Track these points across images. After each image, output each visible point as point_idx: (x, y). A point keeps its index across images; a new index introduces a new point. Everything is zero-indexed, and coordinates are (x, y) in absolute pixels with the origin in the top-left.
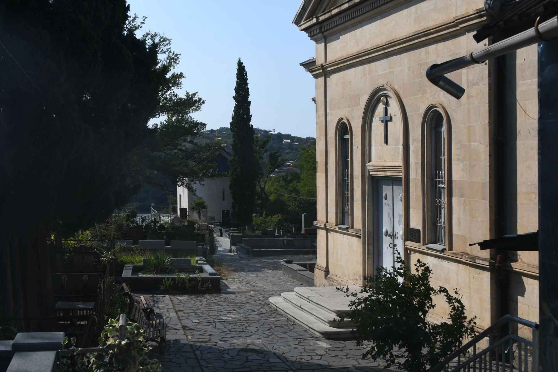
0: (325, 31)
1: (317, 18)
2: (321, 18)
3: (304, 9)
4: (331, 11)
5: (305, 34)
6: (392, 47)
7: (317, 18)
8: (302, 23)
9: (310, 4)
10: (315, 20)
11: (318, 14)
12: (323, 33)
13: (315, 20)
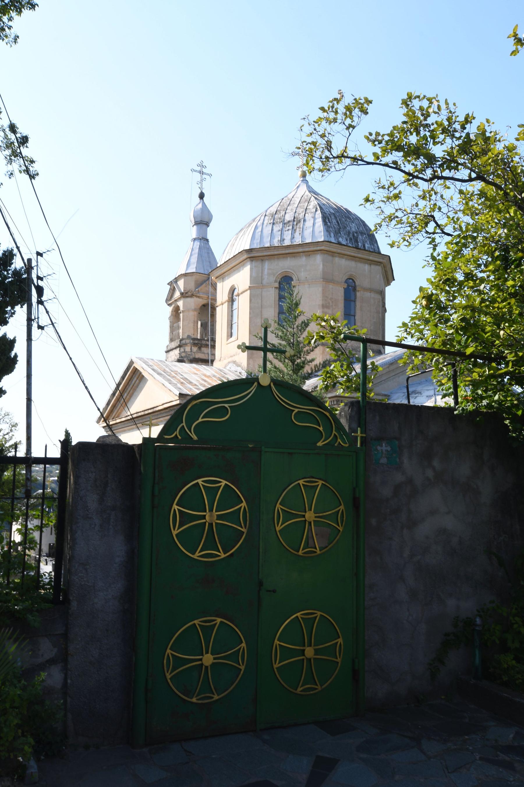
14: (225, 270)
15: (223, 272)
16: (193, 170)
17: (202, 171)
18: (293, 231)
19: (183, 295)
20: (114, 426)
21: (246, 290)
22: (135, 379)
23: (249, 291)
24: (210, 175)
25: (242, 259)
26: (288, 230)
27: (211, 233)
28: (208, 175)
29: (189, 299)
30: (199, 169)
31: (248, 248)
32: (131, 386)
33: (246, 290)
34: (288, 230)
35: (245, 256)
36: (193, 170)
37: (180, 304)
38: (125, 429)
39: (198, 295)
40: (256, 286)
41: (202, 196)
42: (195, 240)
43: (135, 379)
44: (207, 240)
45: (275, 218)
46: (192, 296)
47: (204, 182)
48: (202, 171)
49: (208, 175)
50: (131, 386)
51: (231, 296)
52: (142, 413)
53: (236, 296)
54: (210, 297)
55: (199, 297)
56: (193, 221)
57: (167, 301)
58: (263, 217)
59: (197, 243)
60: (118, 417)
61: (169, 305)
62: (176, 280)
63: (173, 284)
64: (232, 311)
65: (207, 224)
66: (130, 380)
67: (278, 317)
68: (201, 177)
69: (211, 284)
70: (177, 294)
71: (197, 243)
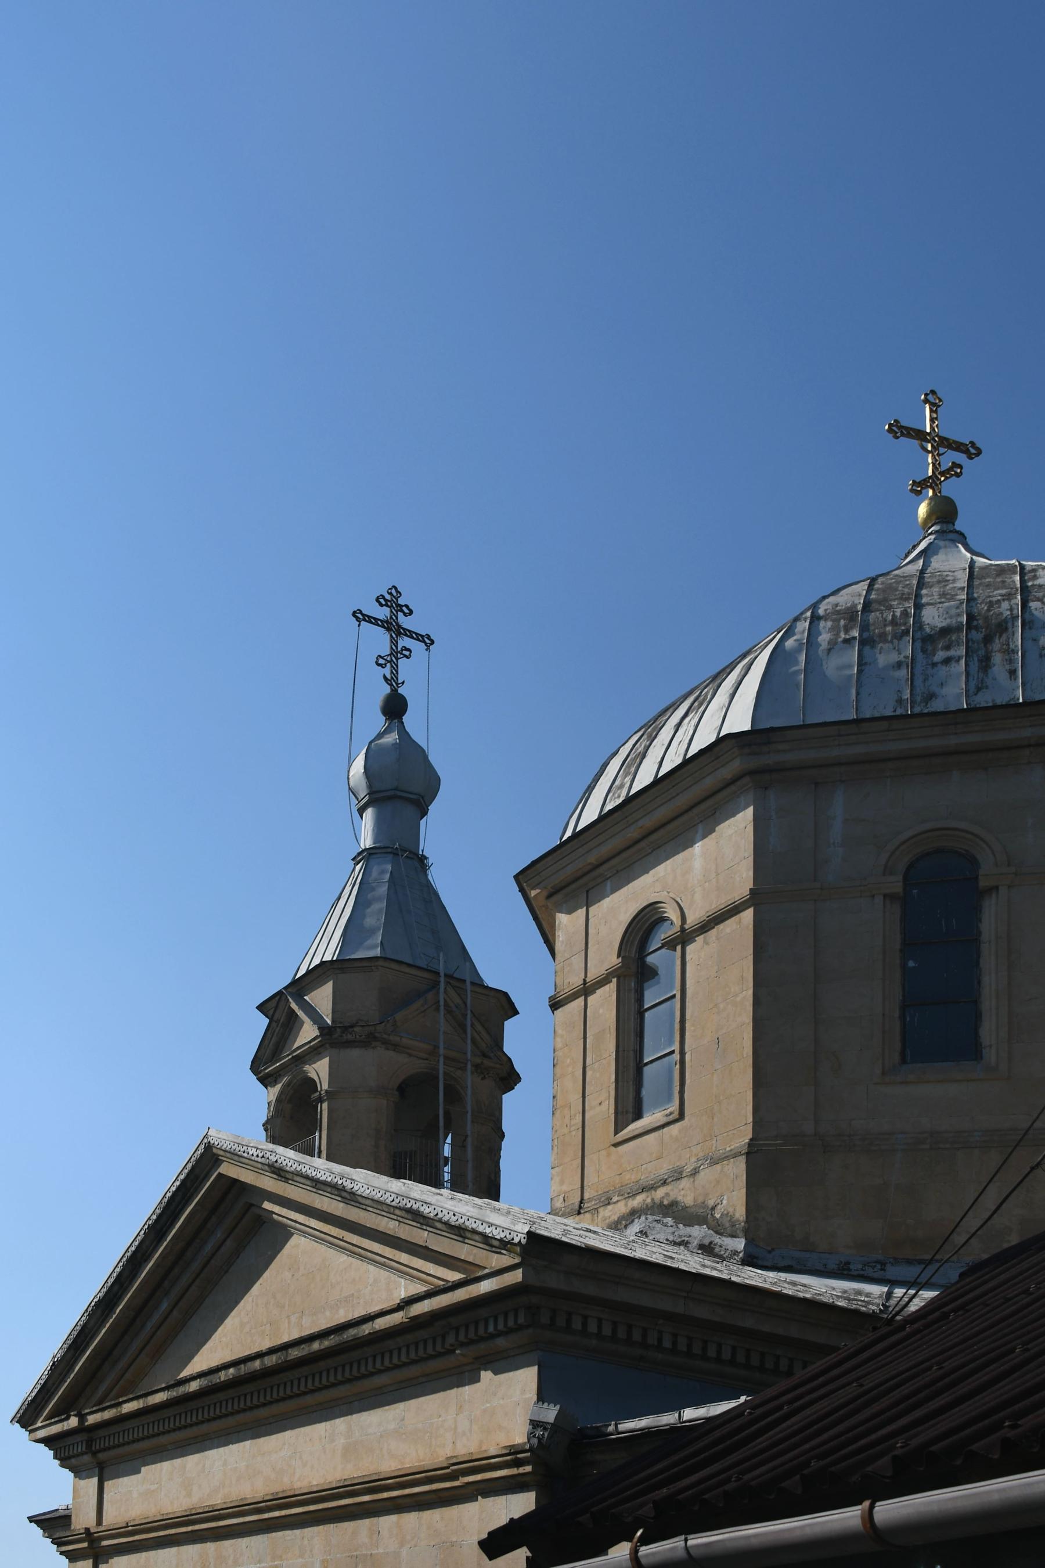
0: (100, 1451)
1: (82, 1418)
2: (91, 1419)
3: (45, 1391)
4: (120, 1404)
5: (46, 1453)
6: (280, 1507)
7: (82, 1418)
8: (39, 1424)
9: (63, 1381)
10: (73, 1422)
11: (83, 1408)
12: (94, 1454)
13: (73, 1422)
14: (606, 849)
15: (592, 858)
16: (360, 616)
17: (392, 616)
18: (975, 666)
19: (331, 1038)
20: (102, 1433)
21: (733, 911)
22: (219, 1235)
23: (748, 916)
24: (427, 641)
25: (726, 772)
26: (947, 661)
27: (437, 835)
28: (419, 637)
29: (355, 1053)
30: (382, 613)
31: (747, 726)
32: (195, 1266)
33: (733, 911)
34: (947, 661)
35: (735, 766)
36: (360, 616)
37: (320, 1070)
38: (163, 1439)
39: (394, 1039)
40: (777, 897)
41: (395, 707)
42: (366, 856)
43: (219, 1235)
44: (422, 859)
45: (865, 625)
46: (369, 1041)
47: (402, 662)
48: (392, 616)
49: (419, 637)
50: (195, 1266)
51: (633, 953)
52: (271, 1361)
53: (669, 945)
54: (442, 1051)
55: (396, 1047)
56: (363, 792)
57: (256, 1066)
58: (803, 626)
59: (384, 870)
60: (130, 1391)
61: (266, 1081)
62: (300, 986)
63: (281, 1011)
64: (641, 1014)
65: (421, 805)
66: (189, 1244)
67: (902, 1017)
68: (394, 642)
69: (446, 1005)
70: (308, 1033)
71: (384, 870)
